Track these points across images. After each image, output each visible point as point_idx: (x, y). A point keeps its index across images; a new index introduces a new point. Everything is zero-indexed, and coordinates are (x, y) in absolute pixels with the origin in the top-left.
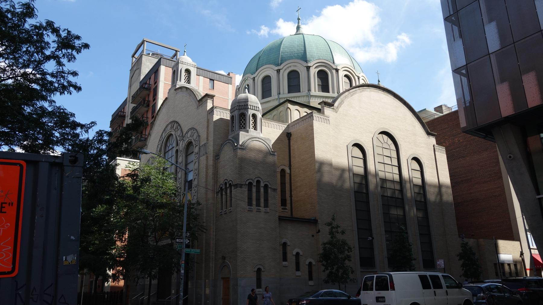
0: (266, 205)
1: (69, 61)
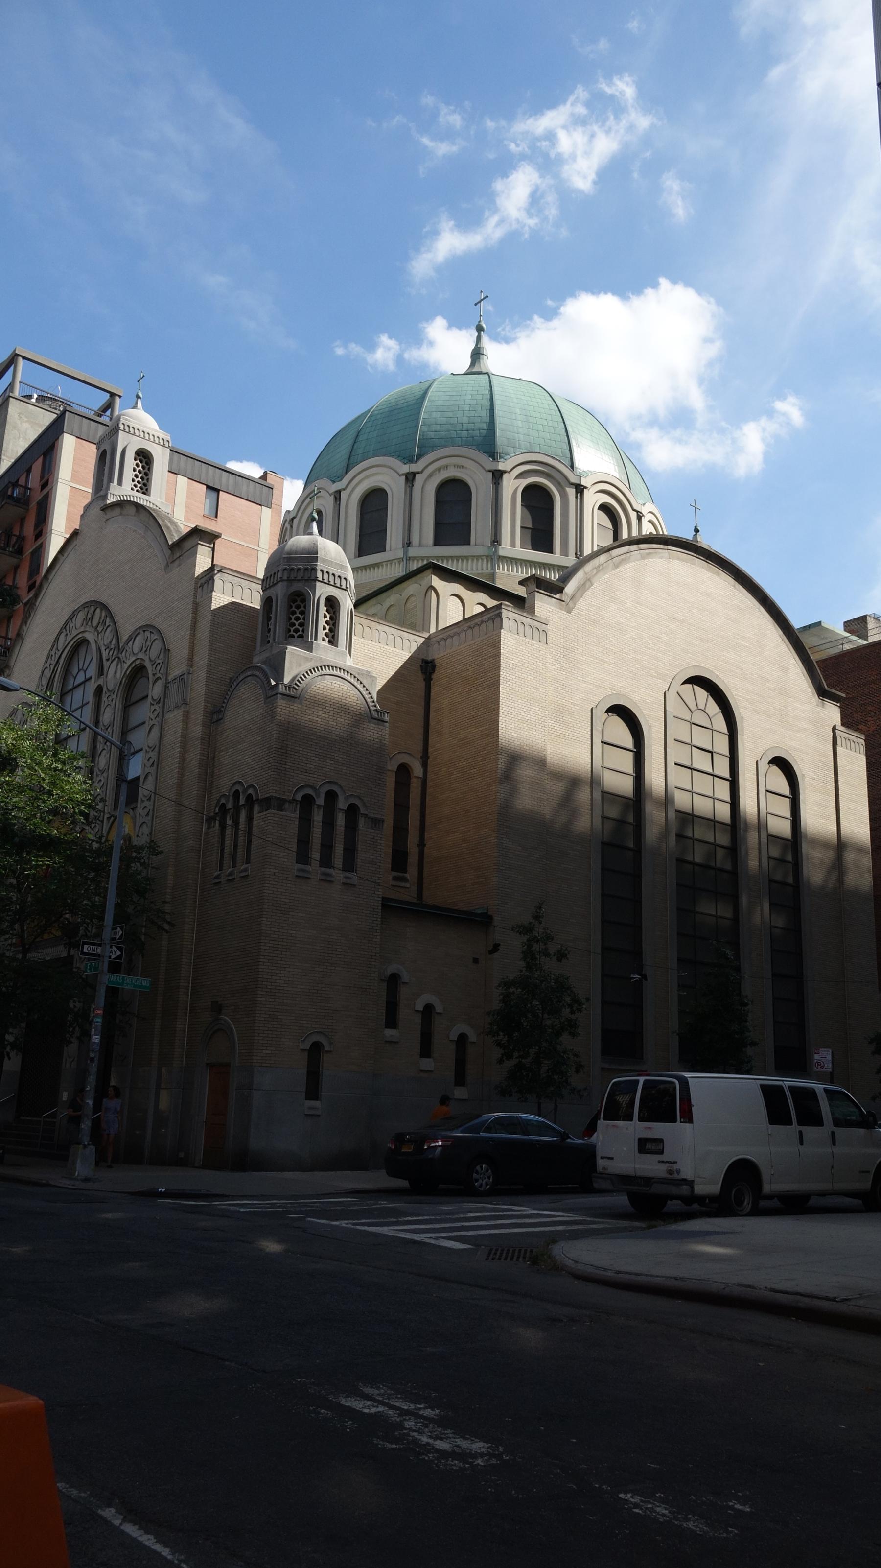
0: (349, 865)
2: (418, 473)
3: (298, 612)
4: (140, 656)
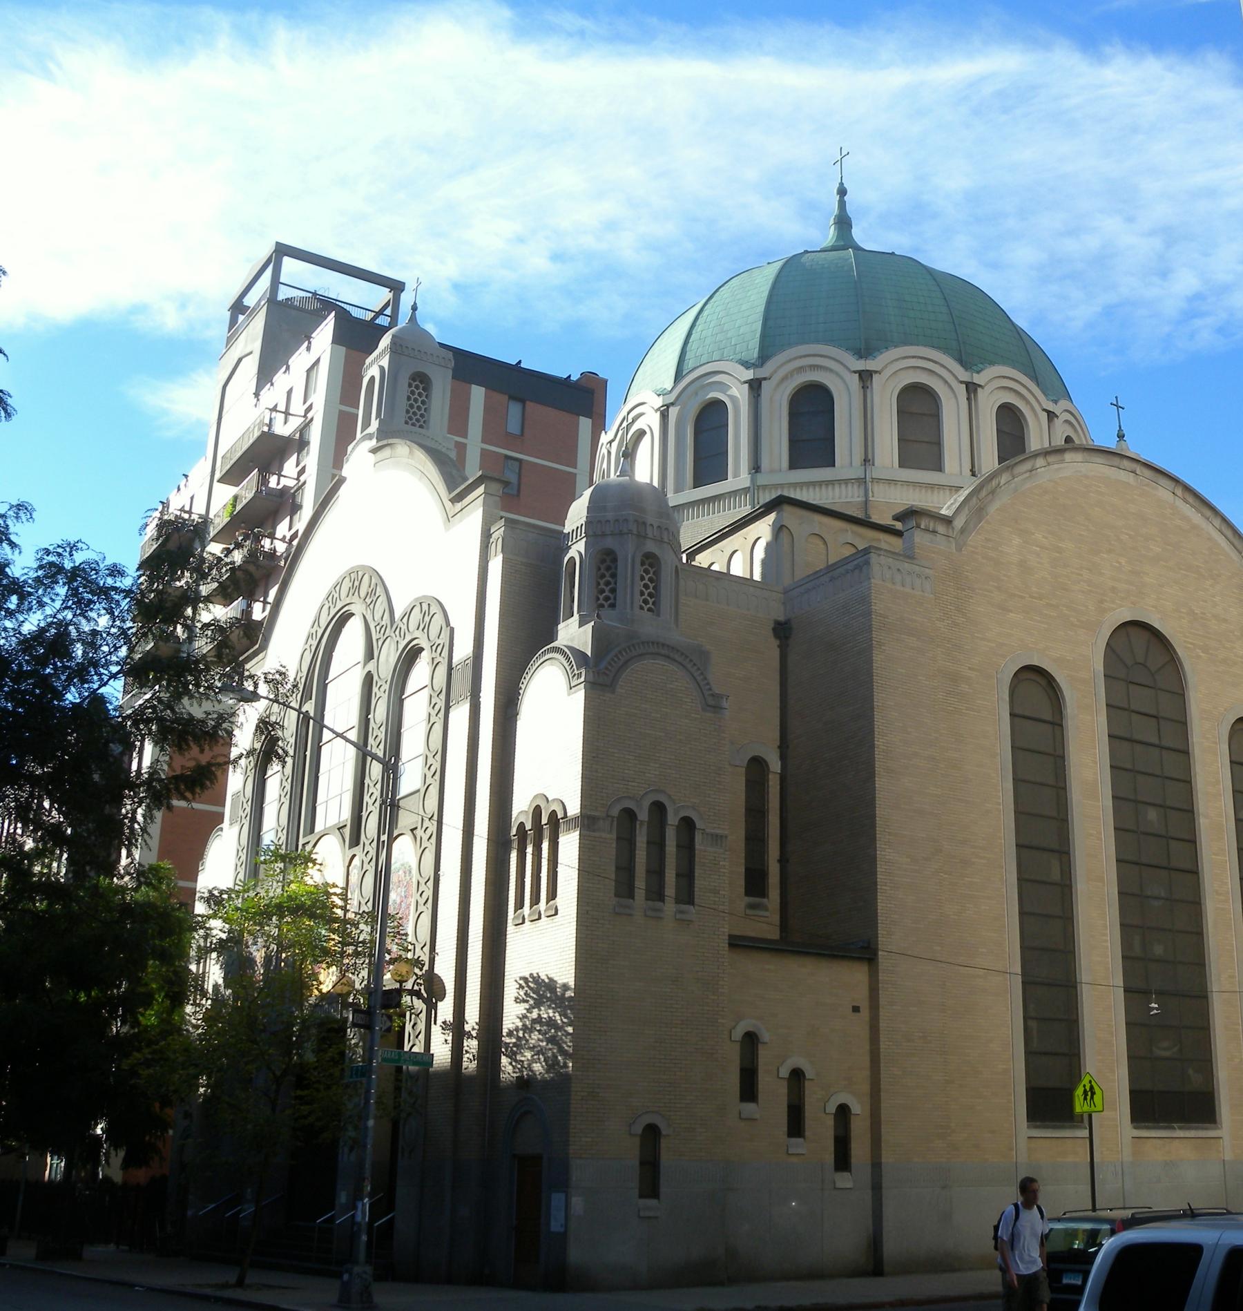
0: (687, 895)
1: (584, 398)
2: (765, 379)
3: (607, 574)
4: (417, 634)
